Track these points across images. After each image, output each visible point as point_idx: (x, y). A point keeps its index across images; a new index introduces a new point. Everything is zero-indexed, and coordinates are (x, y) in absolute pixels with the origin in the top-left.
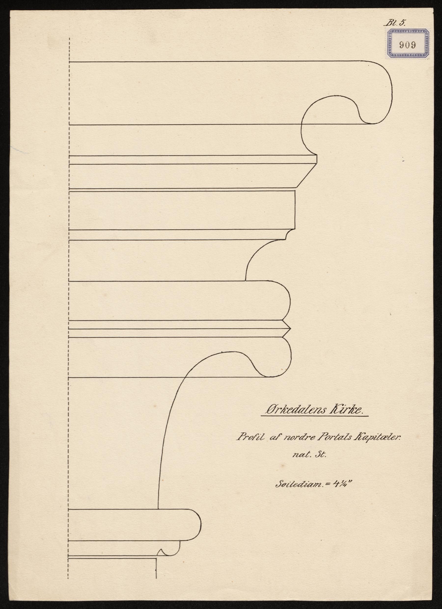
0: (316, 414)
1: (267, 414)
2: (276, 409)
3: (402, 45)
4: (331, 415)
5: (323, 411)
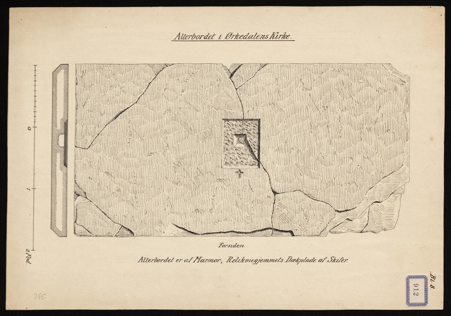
0: (261, 39)
1: (226, 40)
2: (232, 36)
3: (416, 285)
4: (270, 40)
5: (266, 37)
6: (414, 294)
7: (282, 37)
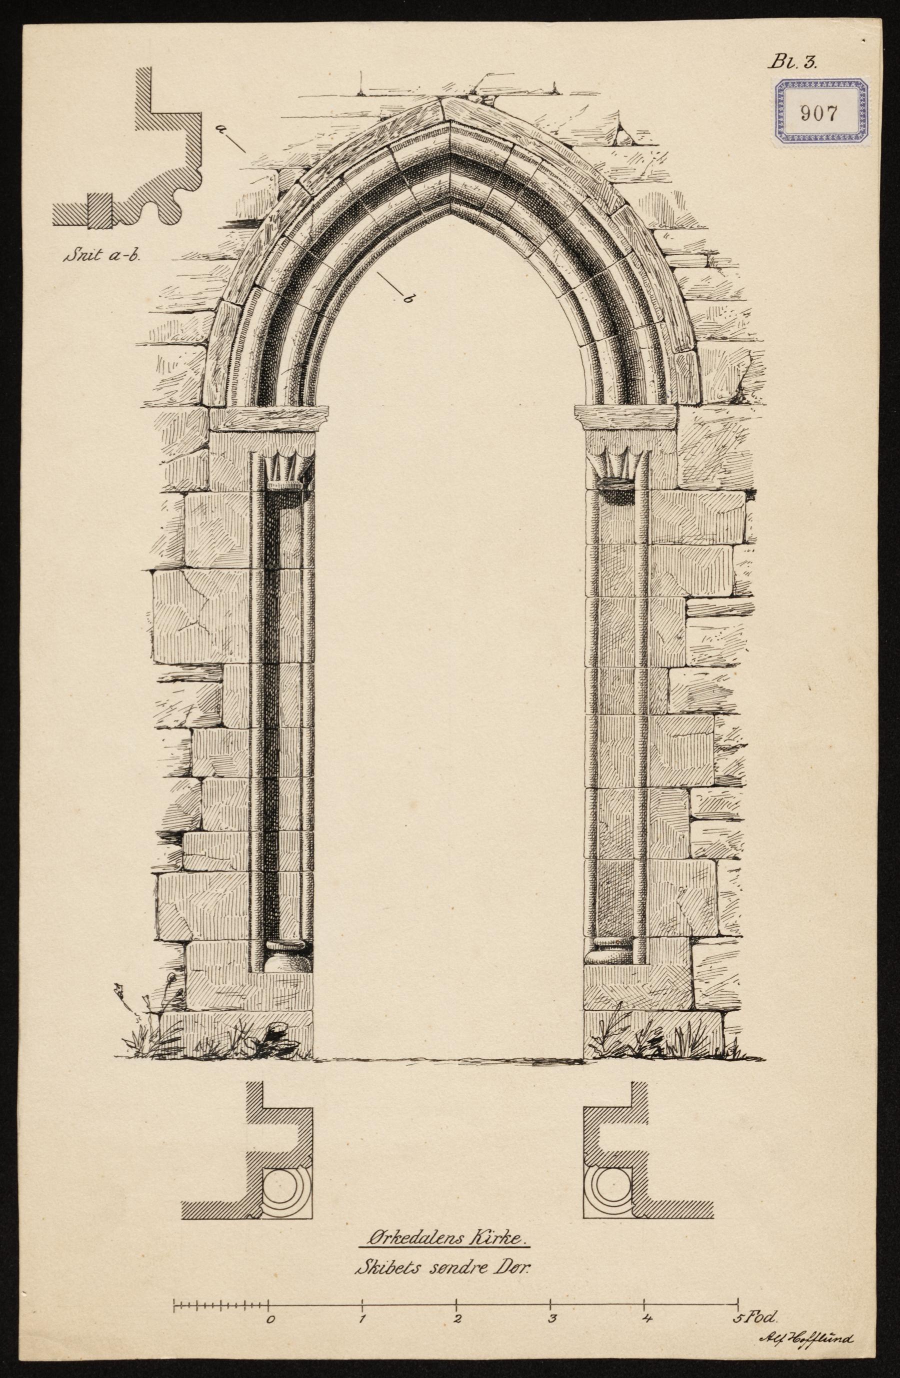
1: (370, 1245)
2: (384, 1238)
6: (832, 107)
7: (499, 1239)
